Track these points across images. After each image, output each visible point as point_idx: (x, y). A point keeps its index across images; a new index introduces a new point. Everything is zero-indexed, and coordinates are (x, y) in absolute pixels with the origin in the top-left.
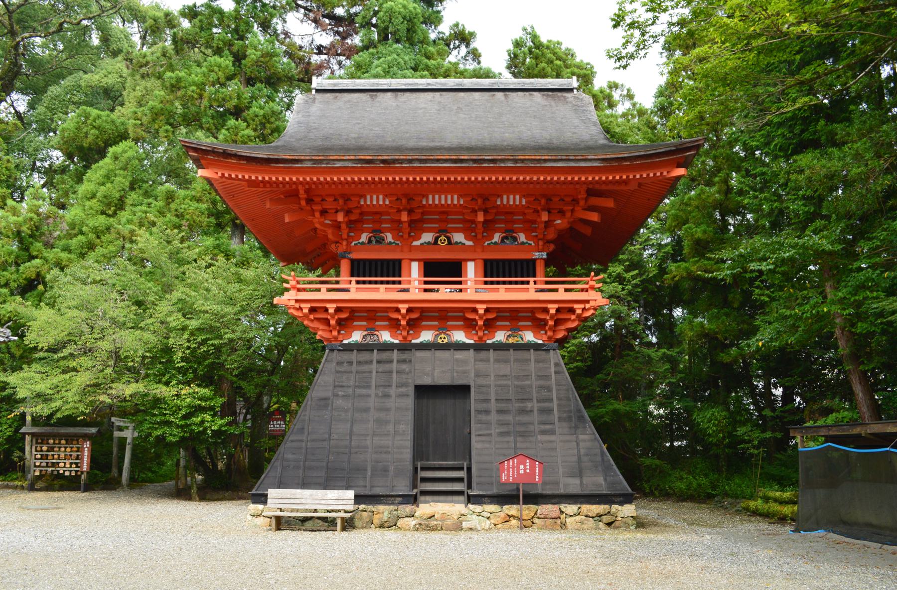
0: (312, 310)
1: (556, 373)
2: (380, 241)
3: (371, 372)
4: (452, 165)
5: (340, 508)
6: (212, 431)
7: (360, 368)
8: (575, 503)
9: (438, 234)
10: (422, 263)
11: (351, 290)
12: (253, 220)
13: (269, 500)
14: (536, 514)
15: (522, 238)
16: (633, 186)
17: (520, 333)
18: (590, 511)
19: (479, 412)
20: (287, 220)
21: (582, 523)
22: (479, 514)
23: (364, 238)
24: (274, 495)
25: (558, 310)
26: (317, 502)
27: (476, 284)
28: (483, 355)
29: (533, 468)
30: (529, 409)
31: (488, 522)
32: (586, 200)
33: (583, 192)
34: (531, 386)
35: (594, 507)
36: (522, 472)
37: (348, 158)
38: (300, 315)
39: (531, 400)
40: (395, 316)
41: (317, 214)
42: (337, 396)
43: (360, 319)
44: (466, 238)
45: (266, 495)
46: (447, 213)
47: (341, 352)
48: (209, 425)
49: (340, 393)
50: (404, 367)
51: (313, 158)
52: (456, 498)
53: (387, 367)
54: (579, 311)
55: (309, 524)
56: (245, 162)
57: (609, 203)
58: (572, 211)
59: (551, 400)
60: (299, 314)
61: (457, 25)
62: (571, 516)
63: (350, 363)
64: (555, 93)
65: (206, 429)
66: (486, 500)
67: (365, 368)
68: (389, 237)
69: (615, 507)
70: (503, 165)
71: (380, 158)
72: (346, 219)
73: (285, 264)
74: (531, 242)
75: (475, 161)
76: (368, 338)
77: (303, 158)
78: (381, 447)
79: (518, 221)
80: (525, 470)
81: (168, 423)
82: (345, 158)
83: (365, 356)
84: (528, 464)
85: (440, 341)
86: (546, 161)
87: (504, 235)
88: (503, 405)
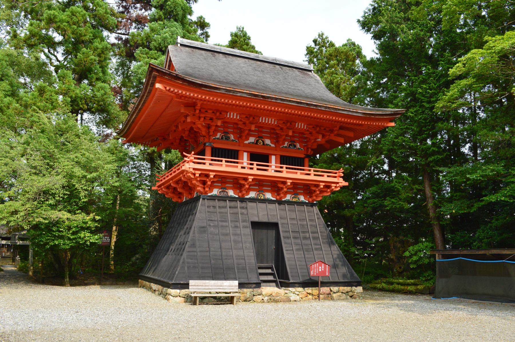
1: (318, 218)
2: (228, 138)
5: (231, 291)
6: (90, 242)
9: (257, 139)
13: (190, 287)
15: (298, 146)
18: (344, 290)
19: (284, 237)
22: (294, 293)
24: (193, 284)
26: (218, 287)
28: (282, 206)
33: (338, 127)
35: (345, 288)
36: (320, 270)
38: (193, 177)
42: (210, 225)
43: (229, 183)
45: (188, 284)
47: (209, 200)
48: (88, 239)
49: (211, 224)
51: (227, 88)
52: (271, 284)
53: (235, 210)
55: (206, 301)
56: (187, 84)
60: (192, 177)
61: (201, 17)
62: (335, 293)
63: (214, 207)
64: (304, 71)
65: (86, 241)
66: (297, 285)
68: (232, 137)
69: (354, 288)
70: (320, 108)
75: (307, 104)
77: (221, 87)
78: (239, 256)
80: (322, 269)
81: (62, 237)
82: (244, 91)
83: (222, 203)
85: (259, 198)
86: (339, 110)
87: (290, 143)
88: (297, 235)
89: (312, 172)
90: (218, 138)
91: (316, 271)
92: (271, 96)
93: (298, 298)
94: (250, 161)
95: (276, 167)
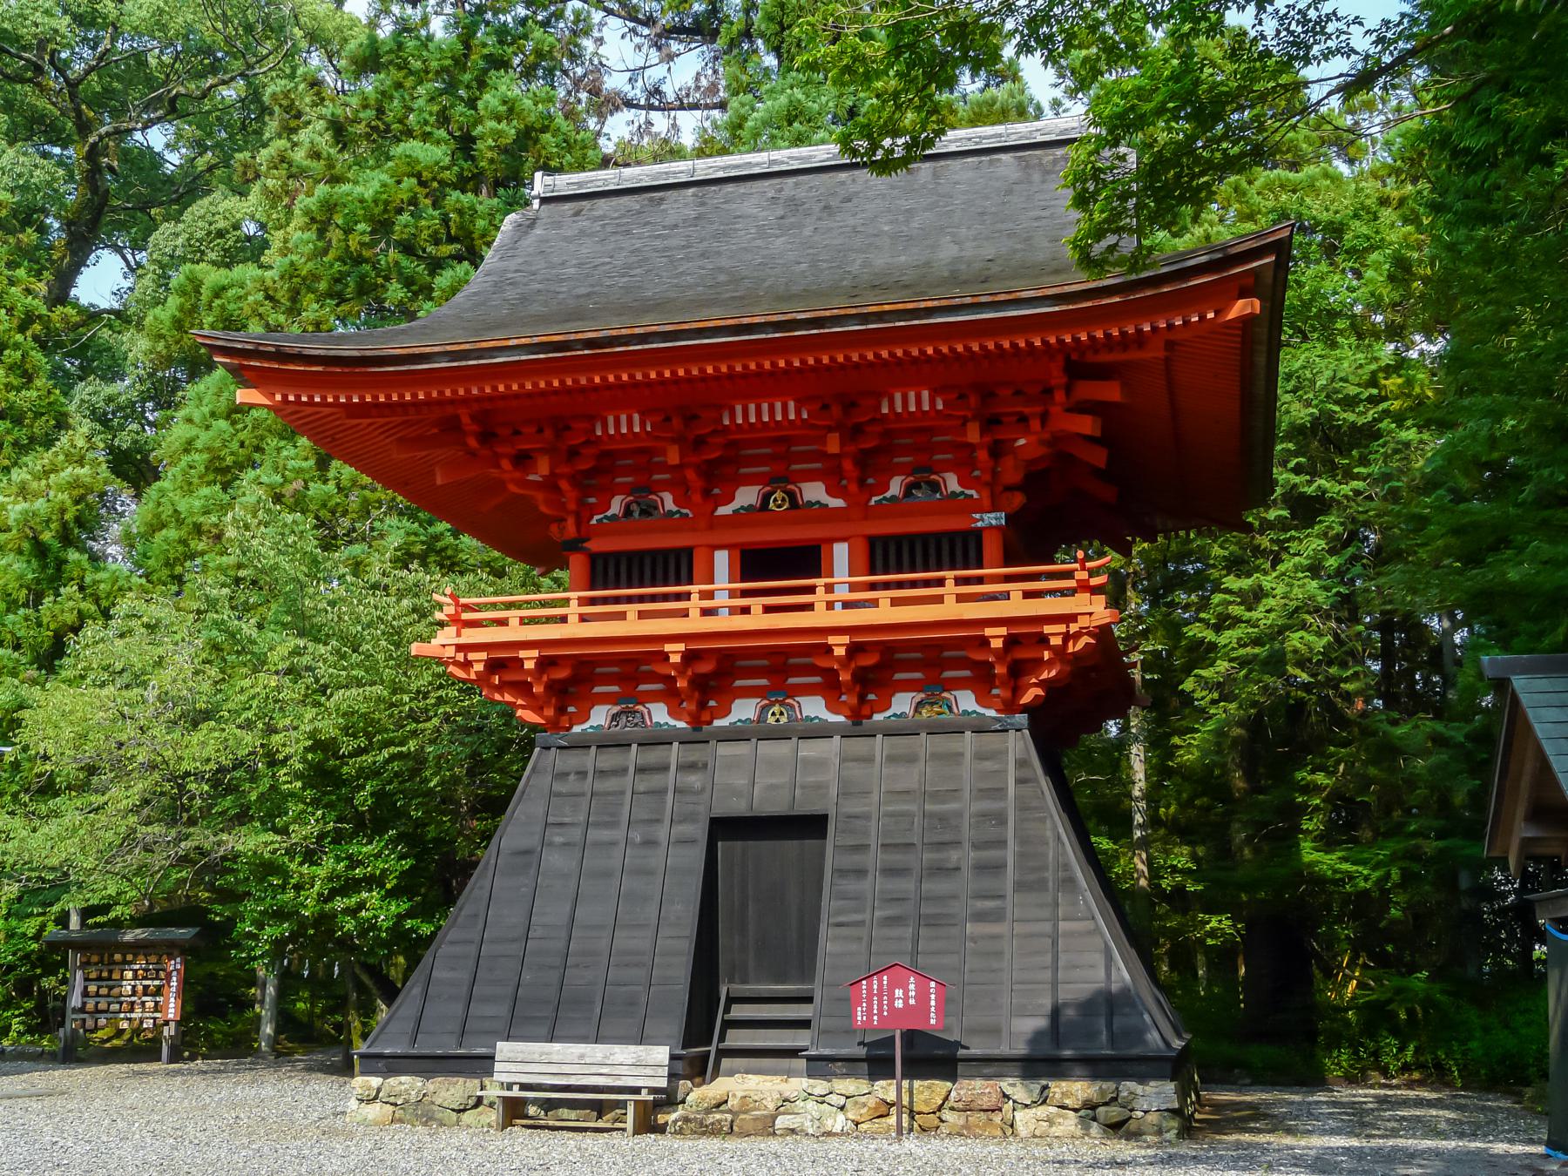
0: (493, 666)
1: (1020, 781)
3: (623, 793)
4: (1064, 308)
7: (601, 786)
10: (737, 553)
11: (511, 622)
12: (407, 484)
13: (498, 1066)
14: (946, 1098)
15: (952, 483)
16: (1154, 352)
17: (945, 695)
19: (841, 872)
20: (439, 482)
21: (1050, 1121)
23: (616, 506)
25: (1010, 641)
26: (594, 1069)
27: (956, 585)
29: (923, 997)
30: (950, 866)
31: (841, 1117)
32: (1068, 389)
34: (959, 814)
36: (899, 1004)
37: (515, 342)
39: (957, 844)
40: (823, 663)
41: (506, 464)
44: (829, 492)
45: (492, 1058)
46: (787, 441)
47: (565, 751)
50: (694, 780)
51: (449, 348)
52: (785, 1063)
53: (655, 780)
54: (1056, 641)
57: (1111, 392)
58: (1044, 418)
59: (1002, 843)
62: (1026, 1106)
66: (1011, 1068)
67: (611, 784)
69: (1129, 1086)
71: (580, 336)
72: (987, 439)
73: (542, 570)
74: (972, 492)
76: (925, 713)
79: (944, 446)
80: (906, 999)
82: (511, 343)
83: (609, 759)
84: (912, 987)
88: (897, 858)
89: (573, 610)
90: (893, 497)
92: (614, 333)
93: (839, 1122)
94: (742, 581)
95: (853, 587)
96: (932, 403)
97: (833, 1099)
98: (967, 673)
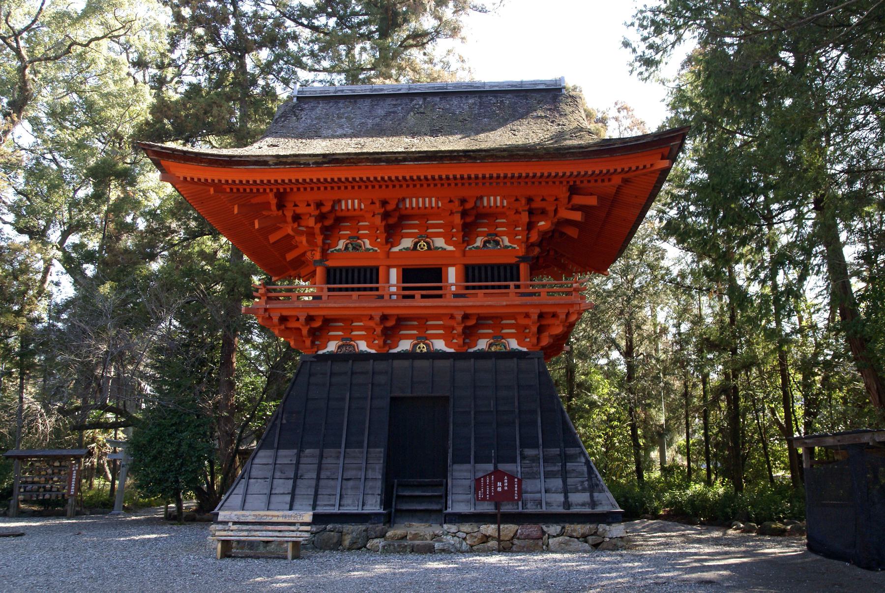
8: (557, 523)
11: (323, 298)
15: (506, 241)
17: (503, 341)
36: (499, 489)
57: (592, 201)
58: (556, 211)
69: (601, 527)
74: (515, 246)
80: (503, 487)
84: (506, 481)
90: (477, 247)
91: (490, 492)
96: (502, 202)
97: (461, 534)
98: (441, 332)
